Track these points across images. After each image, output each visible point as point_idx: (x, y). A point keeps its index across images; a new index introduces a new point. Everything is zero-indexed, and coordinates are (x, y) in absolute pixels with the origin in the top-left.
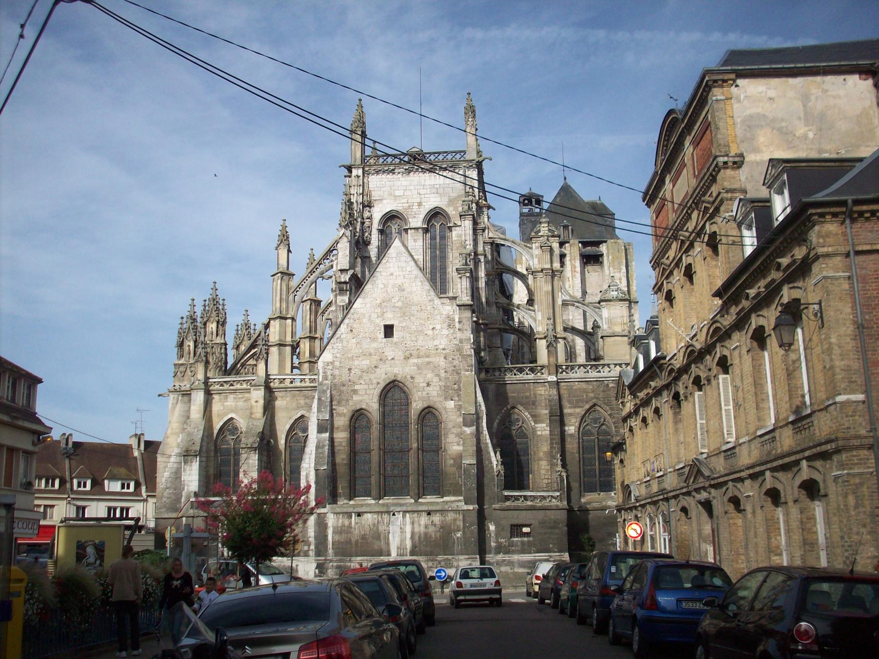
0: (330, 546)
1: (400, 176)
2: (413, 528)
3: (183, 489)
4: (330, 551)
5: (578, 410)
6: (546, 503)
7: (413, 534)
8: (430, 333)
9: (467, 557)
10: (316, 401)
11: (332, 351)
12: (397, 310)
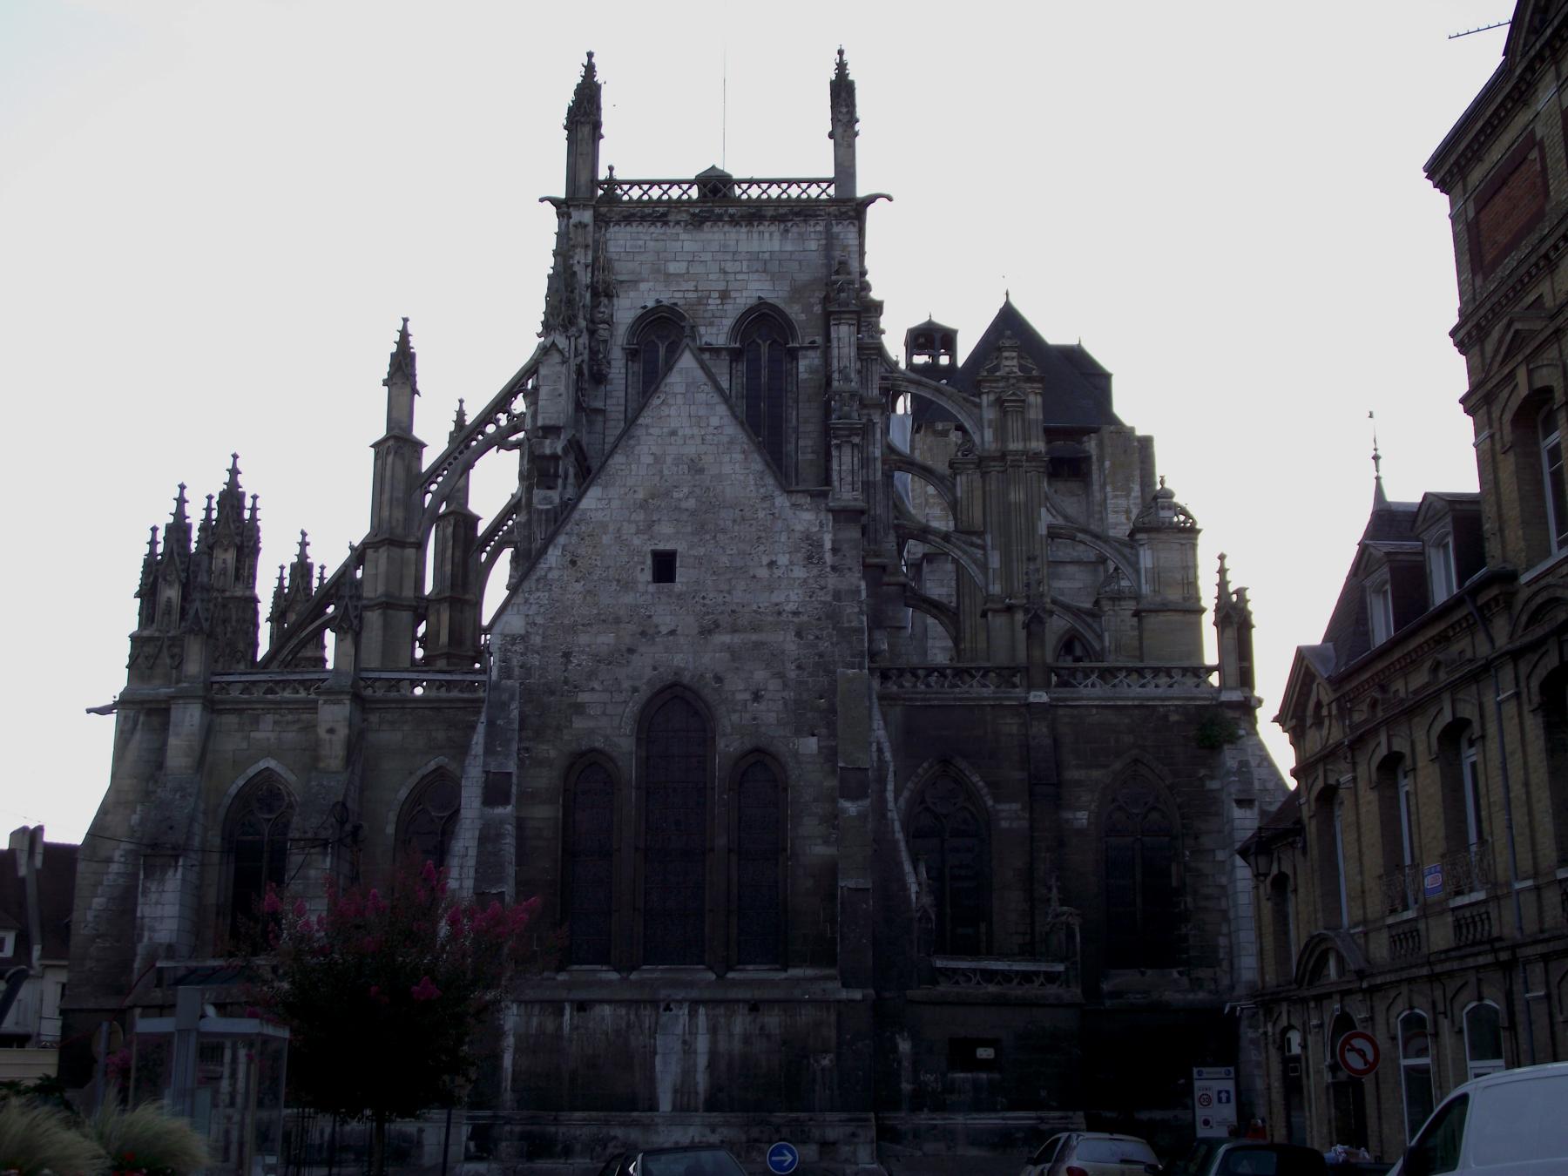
0: (507, 1083)
1: (678, 229)
2: (714, 1043)
3: (140, 937)
4: (508, 1096)
5: (1096, 774)
6: (1033, 990)
7: (713, 1055)
8: (763, 573)
9: (844, 1115)
10: (481, 728)
11: (524, 609)
12: (684, 517)
